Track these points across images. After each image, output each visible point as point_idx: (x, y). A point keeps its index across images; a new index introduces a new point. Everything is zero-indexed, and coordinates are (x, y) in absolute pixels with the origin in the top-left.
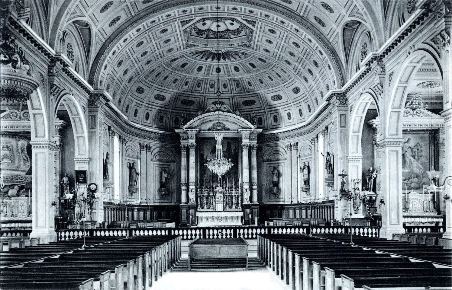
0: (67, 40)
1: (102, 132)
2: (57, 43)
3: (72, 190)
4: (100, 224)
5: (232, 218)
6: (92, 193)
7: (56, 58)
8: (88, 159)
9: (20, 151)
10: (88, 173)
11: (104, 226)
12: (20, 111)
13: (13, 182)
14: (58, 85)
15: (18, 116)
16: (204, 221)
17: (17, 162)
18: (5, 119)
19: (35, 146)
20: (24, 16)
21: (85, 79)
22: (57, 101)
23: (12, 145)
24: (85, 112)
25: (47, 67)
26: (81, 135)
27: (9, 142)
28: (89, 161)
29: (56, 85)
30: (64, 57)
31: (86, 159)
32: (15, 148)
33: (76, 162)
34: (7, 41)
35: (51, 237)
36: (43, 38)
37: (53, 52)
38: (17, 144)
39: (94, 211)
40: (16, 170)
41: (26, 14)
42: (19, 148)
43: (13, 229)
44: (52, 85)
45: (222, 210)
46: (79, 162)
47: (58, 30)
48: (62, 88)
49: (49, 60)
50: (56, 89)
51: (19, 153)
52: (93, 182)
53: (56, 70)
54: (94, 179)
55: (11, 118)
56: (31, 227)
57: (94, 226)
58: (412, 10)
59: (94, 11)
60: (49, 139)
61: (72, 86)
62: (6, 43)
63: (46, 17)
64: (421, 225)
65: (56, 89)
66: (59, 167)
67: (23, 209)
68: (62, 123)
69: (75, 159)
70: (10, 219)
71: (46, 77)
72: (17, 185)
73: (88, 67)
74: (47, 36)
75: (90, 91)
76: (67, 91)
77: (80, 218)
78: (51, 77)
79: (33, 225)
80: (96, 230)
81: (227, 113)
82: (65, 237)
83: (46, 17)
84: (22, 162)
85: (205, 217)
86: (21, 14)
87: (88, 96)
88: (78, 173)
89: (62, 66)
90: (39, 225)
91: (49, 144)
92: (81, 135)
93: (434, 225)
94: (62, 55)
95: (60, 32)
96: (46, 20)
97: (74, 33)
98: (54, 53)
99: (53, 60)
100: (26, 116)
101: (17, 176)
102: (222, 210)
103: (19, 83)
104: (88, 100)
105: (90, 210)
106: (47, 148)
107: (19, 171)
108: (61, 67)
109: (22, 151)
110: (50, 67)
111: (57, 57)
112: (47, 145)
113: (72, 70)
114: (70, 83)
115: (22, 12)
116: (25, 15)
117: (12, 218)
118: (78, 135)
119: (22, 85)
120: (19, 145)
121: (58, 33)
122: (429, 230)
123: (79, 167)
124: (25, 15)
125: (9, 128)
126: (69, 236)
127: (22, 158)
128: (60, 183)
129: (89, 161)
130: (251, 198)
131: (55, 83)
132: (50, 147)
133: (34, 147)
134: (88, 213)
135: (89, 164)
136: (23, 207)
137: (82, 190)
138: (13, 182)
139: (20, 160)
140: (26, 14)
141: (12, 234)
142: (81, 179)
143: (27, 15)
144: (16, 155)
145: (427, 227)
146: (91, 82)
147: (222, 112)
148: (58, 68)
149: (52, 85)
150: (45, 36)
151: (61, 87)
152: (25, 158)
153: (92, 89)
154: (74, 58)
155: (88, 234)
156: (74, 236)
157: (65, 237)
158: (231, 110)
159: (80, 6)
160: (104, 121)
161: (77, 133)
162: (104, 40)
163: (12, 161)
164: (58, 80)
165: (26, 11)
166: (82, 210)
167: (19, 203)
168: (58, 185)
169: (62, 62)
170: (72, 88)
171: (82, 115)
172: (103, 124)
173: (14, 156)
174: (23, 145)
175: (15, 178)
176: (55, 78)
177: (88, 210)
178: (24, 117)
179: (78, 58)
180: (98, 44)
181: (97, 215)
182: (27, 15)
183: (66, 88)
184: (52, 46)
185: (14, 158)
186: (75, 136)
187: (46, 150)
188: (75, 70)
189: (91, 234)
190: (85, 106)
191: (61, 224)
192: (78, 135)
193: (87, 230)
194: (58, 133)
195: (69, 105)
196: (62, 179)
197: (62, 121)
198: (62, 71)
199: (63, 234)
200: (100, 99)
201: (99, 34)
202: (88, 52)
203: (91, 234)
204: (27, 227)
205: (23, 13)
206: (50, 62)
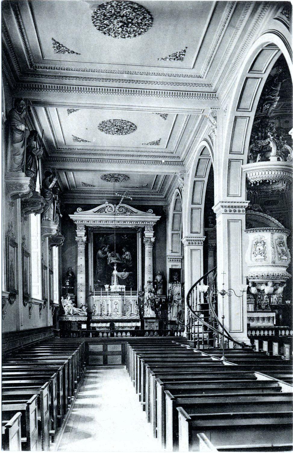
5: (263, 319)
16: (260, 321)
31: (179, 257)
45: (253, 310)
55: (106, 212)
58: (5, 75)
64: (120, 329)
67: (117, 307)
68: (159, 219)
70: (106, 318)
81: (258, 212)
85: (267, 318)
93: (133, 329)
100: (121, 210)
102: (253, 310)
122: (128, 334)
125: (110, 223)
135: (181, 262)
136: (117, 305)
141: (126, 334)
142: (175, 278)
145: (126, 332)
147: (254, 212)
155: (274, 333)
158: (262, 210)
167: (113, 302)
178: (119, 211)
192: (173, 232)
194: (153, 229)
204: (125, 327)
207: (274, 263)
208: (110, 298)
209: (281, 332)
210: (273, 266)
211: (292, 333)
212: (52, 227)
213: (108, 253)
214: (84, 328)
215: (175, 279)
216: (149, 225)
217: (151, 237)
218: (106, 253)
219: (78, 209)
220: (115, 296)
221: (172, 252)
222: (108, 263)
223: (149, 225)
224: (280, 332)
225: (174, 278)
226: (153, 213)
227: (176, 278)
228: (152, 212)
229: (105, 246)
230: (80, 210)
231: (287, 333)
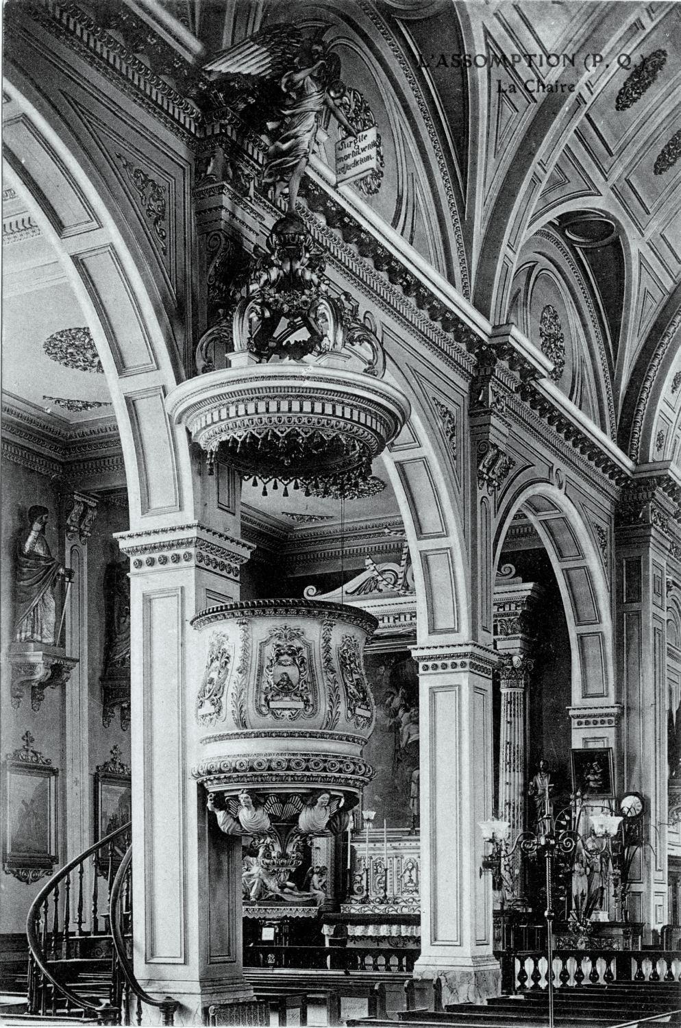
0: (543, 295)
1: (665, 615)
2: (499, 297)
3: (562, 818)
4: (655, 931)
6: (634, 830)
7: (494, 346)
8: (615, 710)
9: (336, 664)
10: (613, 757)
11: (669, 938)
12: (403, 563)
13: (310, 779)
14: (502, 447)
15: (400, 581)
17: (324, 707)
18: (362, 596)
19: (430, 663)
20: (356, 163)
21: (603, 429)
22: (502, 509)
23: (308, 645)
24: (603, 546)
25: (464, 385)
26: (592, 629)
27: (297, 635)
28: (619, 717)
29: (495, 446)
30: (524, 341)
32: (318, 651)
33: (574, 722)
34: (297, 265)
35: (479, 980)
36: (451, 279)
37: (482, 326)
38: (327, 641)
39: (635, 887)
40: (322, 736)
41: (364, 155)
42: (333, 654)
43: (385, 946)
44: (480, 446)
46: (590, 720)
47: (504, 248)
48: (520, 462)
49: (473, 357)
50: (494, 461)
51: (333, 671)
52: (632, 790)
53: (495, 393)
54: (635, 781)
55: (380, 591)
56: (417, 940)
57: (635, 942)
59: (631, 168)
60: (474, 636)
61: (557, 452)
62: (293, 272)
63: (462, 210)
65: (494, 461)
66: (521, 743)
68: (529, 593)
69: (571, 713)
70: (377, 911)
71: (463, 421)
72: (327, 791)
73: (616, 389)
74: (466, 272)
75: (621, 471)
76: (540, 471)
77: (588, 913)
78: (479, 421)
79: (424, 931)
80: (640, 958)
82: (536, 976)
83: (462, 210)
84: (342, 708)
86: (347, 157)
87: (613, 487)
88: (587, 757)
89: (517, 375)
90: (441, 936)
91: (472, 655)
92: (592, 629)
94: (515, 331)
95: (510, 253)
96: (462, 219)
97: (567, 269)
98: (488, 328)
99: (488, 356)
101: (325, 758)
103: (329, 410)
104: (616, 504)
105: (620, 887)
106: (467, 668)
107: (332, 736)
108: (514, 380)
109: (343, 665)
110: (477, 384)
111: (495, 341)
112: (467, 660)
113: (548, 387)
114: (547, 444)
115: (348, 151)
116: (362, 161)
117: (382, 907)
118: (584, 629)
119: (339, 413)
120: (332, 643)
121: (501, 256)
123: (585, 740)
124: (362, 161)
126: (564, 975)
127: (341, 692)
128: (524, 794)
129: (619, 717)
130: (355, 938)
131: (492, 439)
132: (477, 665)
133: (426, 668)
134: (615, 895)
136: (414, 872)
137: (600, 821)
138: (310, 779)
139: (334, 701)
140: (364, 155)
143: (369, 158)
144: (323, 685)
146: (624, 438)
148: (506, 388)
149: (480, 446)
150: (457, 270)
151: (516, 458)
152: (353, 689)
153: (629, 463)
154: (567, 357)
156: (579, 975)
157: (536, 976)
159: (580, 152)
160: (671, 578)
161: (579, 621)
162: (669, 284)
163: (306, 702)
164: (505, 430)
165: (362, 145)
166: (597, 884)
168: (519, 800)
169: (517, 361)
170: (558, 464)
171: (594, 563)
172: (669, 589)
173: (313, 682)
174: (348, 642)
175: (316, 764)
176: (494, 420)
177: (616, 886)
179: (583, 362)
180: (649, 301)
181: (644, 903)
182: (369, 158)
183: (535, 461)
184: (482, 307)
185: (315, 691)
186: (573, 631)
187: (463, 679)
188: (570, 398)
189: (624, 968)
190: (605, 527)
191: (519, 932)
192: (584, 629)
193: (608, 957)
195: (552, 524)
196: (531, 779)
197: (530, 585)
198: (518, 396)
199: (529, 966)
200: (658, 496)
201: (650, 257)
202: (616, 329)
203: (624, 968)
205: (354, 154)
206: (476, 367)
207: (244, 725)
208: (395, 848)
209: (522, 964)
210: (247, 736)
211: (676, 968)
212: (32, 660)
213: (401, 712)
214: (263, 934)
215: (591, 784)
216: (508, 615)
217: (511, 652)
218: (396, 713)
219: (305, 591)
220: (408, 844)
221: (585, 696)
222: (403, 744)
223: (508, 615)
224: (518, 963)
225: (589, 780)
226: (514, 576)
227: (595, 780)
228: (514, 572)
229: (395, 692)
230: (311, 593)
231: (662, 968)
